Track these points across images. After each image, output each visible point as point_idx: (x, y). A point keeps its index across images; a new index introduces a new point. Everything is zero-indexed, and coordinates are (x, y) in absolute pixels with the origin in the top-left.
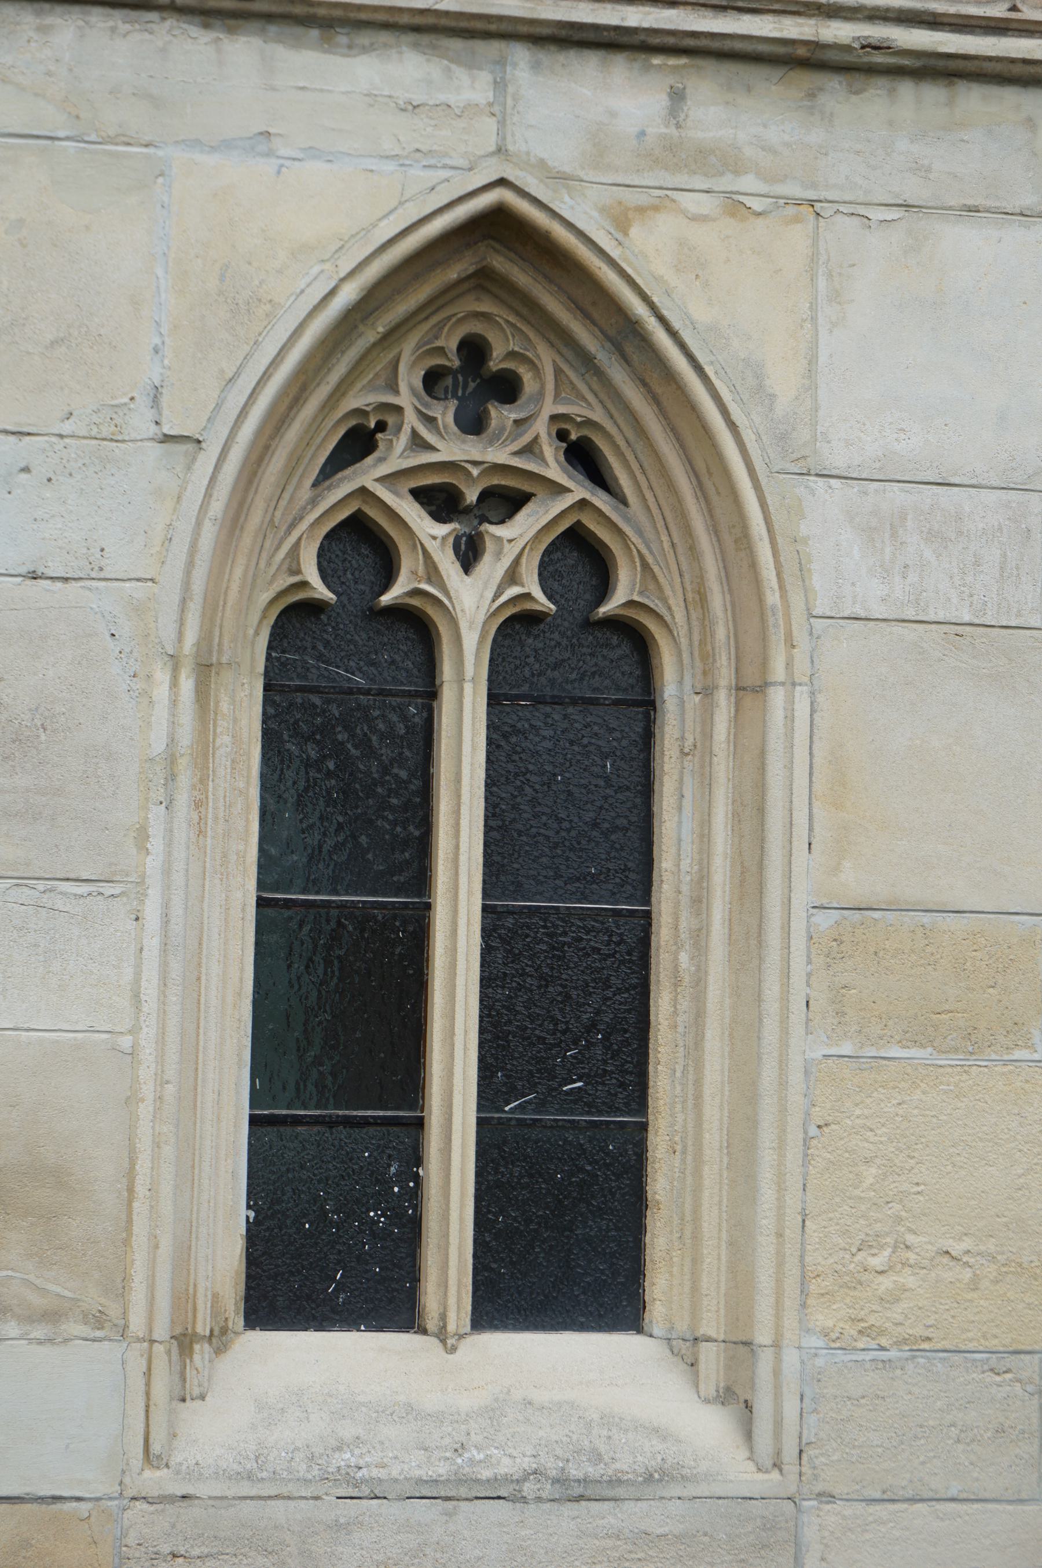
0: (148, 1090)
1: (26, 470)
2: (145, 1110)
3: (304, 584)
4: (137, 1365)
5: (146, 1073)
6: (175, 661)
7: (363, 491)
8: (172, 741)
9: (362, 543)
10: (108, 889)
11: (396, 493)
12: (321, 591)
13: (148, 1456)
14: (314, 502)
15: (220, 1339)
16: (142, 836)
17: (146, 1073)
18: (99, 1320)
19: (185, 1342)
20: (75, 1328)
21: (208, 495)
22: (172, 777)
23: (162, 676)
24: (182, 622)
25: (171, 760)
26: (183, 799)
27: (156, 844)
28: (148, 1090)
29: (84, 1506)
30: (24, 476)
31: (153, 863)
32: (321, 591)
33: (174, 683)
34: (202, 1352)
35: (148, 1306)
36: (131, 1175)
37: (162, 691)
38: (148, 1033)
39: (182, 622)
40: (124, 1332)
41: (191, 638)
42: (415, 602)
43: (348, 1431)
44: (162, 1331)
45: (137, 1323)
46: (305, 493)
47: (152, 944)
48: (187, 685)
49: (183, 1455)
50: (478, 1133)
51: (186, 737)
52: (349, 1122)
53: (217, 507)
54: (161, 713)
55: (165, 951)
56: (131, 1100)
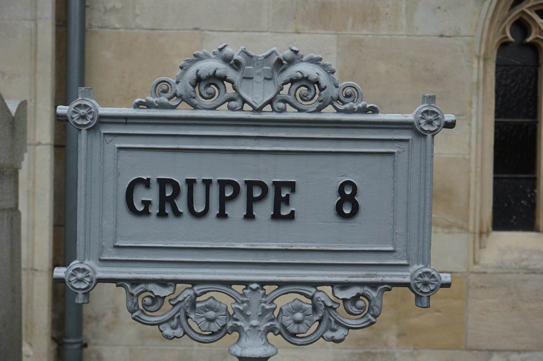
0: (473, 169)
1: (439, 8)
2: (473, 174)
3: (507, 37)
4: (471, 239)
5: (473, 165)
6: (479, 58)
7: (523, 12)
8: (478, 78)
9: (522, 26)
10: (462, 117)
11: (531, 12)
12: (511, 39)
13: (475, 263)
14: (509, 15)
15: (488, 233)
16: (471, 103)
17: (473, 165)
18: (461, 228)
19: (481, 233)
20: (456, 230)
21: (487, 13)
22: (478, 88)
23: (475, 61)
24: (480, 47)
25: (478, 83)
26: (481, 93)
27: (474, 105)
28: (473, 169)
29: (458, 275)
30: (438, 10)
31: (474, 111)
32: (511, 39)
33: (479, 63)
34: (484, 236)
35: (473, 224)
36: (469, 191)
37: (475, 65)
38: (473, 154)
39: (480, 47)
40: (467, 231)
41: (483, 51)
42: (537, 41)
43: (524, 256)
44: (477, 231)
45: (471, 228)
46: (507, 13)
47: (474, 131)
48: (482, 63)
49: (482, 262)
50: (496, 179)
51: (481, 78)
52: (516, 178)
53: (490, 16)
54: (475, 72)
55: (4, 209)
56: (469, 172)
